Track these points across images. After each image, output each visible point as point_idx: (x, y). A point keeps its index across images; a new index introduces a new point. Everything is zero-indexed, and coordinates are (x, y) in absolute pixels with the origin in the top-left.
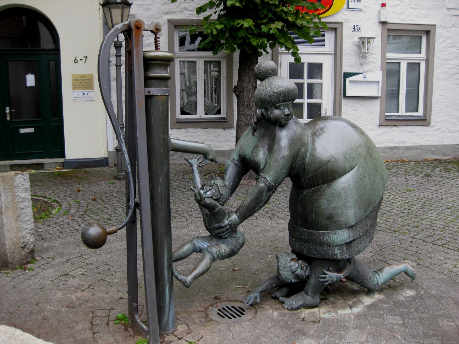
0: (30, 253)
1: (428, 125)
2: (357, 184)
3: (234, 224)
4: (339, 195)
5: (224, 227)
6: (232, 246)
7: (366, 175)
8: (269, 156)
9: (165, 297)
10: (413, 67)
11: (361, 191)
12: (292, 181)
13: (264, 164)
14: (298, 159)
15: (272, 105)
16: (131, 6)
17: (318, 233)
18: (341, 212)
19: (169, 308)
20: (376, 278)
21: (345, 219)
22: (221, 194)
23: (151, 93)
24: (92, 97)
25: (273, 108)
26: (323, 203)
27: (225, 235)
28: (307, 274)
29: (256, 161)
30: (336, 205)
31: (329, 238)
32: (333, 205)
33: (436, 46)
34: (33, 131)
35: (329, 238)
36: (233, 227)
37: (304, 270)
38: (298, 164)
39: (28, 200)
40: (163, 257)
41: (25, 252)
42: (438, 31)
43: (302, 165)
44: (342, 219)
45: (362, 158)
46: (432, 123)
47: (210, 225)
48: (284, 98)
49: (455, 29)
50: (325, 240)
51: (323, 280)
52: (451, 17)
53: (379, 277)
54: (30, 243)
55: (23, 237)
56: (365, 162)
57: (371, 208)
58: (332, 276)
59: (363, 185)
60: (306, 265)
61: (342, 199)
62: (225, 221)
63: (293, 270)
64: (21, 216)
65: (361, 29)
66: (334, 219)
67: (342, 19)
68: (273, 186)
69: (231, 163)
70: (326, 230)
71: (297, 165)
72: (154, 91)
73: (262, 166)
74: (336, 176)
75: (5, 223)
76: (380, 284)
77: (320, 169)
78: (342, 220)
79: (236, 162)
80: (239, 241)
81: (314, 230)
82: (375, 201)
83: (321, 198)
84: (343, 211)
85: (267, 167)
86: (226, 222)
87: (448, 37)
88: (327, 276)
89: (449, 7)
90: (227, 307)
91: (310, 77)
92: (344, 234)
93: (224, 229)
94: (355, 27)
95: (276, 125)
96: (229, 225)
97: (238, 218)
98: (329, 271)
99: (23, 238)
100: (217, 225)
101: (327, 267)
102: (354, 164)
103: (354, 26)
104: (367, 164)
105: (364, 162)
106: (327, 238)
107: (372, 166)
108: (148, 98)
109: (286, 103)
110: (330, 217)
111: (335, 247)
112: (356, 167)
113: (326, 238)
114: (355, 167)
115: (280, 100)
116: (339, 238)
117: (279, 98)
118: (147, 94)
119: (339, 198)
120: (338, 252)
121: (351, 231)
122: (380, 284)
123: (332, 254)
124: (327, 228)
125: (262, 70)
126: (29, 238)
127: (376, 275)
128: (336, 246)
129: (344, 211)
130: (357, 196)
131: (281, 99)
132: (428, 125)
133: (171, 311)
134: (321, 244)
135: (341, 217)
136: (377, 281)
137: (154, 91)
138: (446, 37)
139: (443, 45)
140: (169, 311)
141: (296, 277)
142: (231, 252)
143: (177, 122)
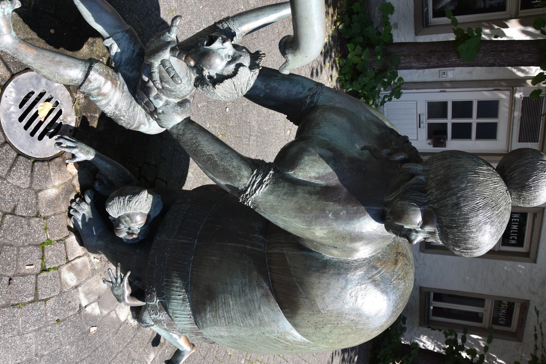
4: (250, 315)
18: (221, 315)
29: (301, 159)
30: (232, 307)
31: (177, 287)
32: (231, 303)
34: (453, 39)
46: (422, 254)
61: (244, 319)
66: (208, 302)
69: (307, 89)
78: (208, 316)
79: (308, 101)
84: (223, 318)
90: (60, 113)
92: (185, 316)
106: (178, 285)
116: (177, 307)
119: (245, 314)
120: (156, 302)
129: (223, 321)
135: (212, 315)
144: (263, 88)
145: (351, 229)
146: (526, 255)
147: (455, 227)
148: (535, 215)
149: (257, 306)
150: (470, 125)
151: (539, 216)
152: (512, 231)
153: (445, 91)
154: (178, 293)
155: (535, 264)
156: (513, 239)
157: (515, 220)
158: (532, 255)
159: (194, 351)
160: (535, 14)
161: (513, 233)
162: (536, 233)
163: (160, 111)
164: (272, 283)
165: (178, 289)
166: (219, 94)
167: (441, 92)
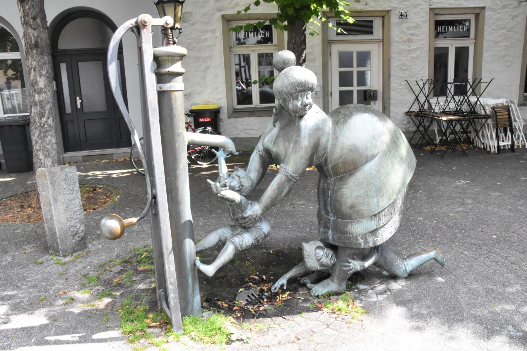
0: (80, 241)
5: (246, 218)
6: (256, 236)
15: (289, 95)
16: (184, 4)
20: (405, 265)
22: (242, 186)
23: (163, 89)
27: (249, 225)
28: (332, 262)
33: (485, 29)
37: (330, 258)
41: (75, 240)
42: (488, 13)
43: (324, 155)
44: (364, 208)
48: (301, 89)
49: (507, 10)
50: (348, 228)
51: (348, 268)
53: (408, 264)
54: (81, 232)
55: (72, 226)
58: (356, 265)
63: (318, 258)
64: (70, 207)
65: (409, 17)
66: (357, 208)
67: (389, 7)
73: (282, 157)
75: (54, 214)
77: (341, 158)
83: (344, 187)
87: (498, 19)
88: (351, 264)
91: (352, 66)
93: (247, 219)
94: (403, 14)
99: (73, 228)
102: (376, 152)
103: (402, 13)
108: (161, 94)
112: (379, 156)
114: (377, 155)
115: (296, 90)
118: (159, 90)
138: (496, 19)
139: (493, 27)
141: (322, 265)
143: (234, 112)
145: (308, 132)
146: (477, 16)
148: (436, 14)
150: (352, 72)
151: (437, 12)
152: (455, 31)
153: (331, 93)
155: (486, 8)
157: (443, 29)
158: (477, 11)
159: (39, 50)
161: (456, 29)
162: (455, 12)
164: (346, 173)
167: (331, 96)
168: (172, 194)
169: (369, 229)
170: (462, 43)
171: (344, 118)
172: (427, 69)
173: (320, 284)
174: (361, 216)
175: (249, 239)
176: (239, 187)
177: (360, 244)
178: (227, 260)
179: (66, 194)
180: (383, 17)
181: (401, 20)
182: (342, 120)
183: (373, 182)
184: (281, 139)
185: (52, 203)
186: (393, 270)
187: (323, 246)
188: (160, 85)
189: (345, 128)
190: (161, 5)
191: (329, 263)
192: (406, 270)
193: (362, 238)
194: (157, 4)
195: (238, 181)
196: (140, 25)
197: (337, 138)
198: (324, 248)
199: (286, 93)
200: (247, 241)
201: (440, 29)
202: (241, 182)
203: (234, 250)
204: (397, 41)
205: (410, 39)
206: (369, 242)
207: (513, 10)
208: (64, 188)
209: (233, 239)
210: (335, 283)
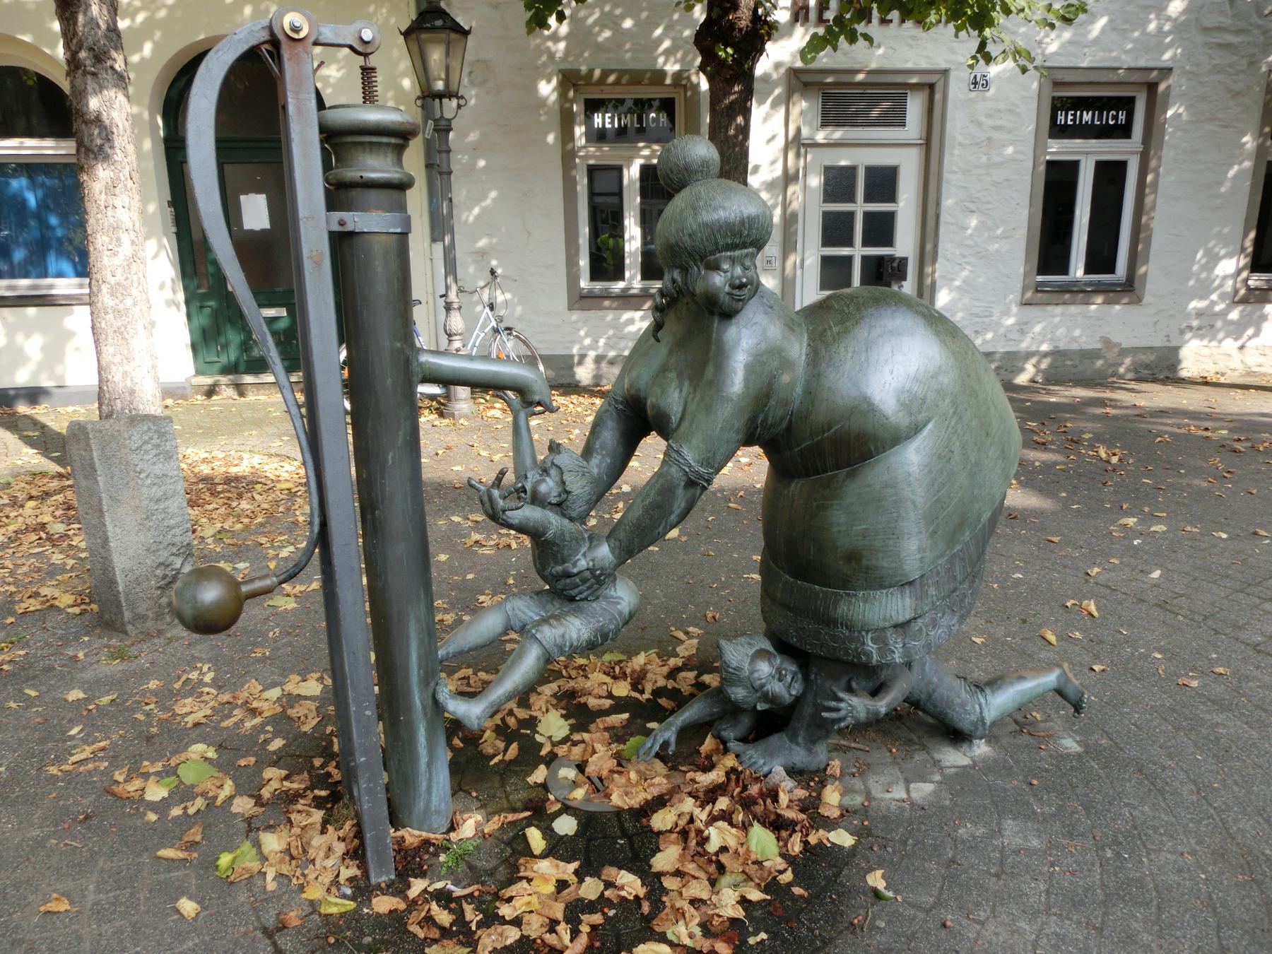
1: (1138, 300)
2: (930, 471)
3: (602, 569)
4: (879, 501)
7: (957, 447)
8: (691, 396)
9: (418, 753)
10: (1110, 174)
11: (938, 492)
12: (768, 454)
13: (679, 416)
14: (772, 402)
15: (697, 257)
17: (823, 592)
19: (430, 779)
21: (894, 565)
22: (568, 493)
24: (1101, 259)
25: (701, 267)
26: (838, 518)
27: (581, 593)
31: (849, 610)
32: (863, 527)
35: (849, 610)
36: (600, 575)
38: (771, 415)
39: (172, 481)
40: (408, 655)
45: (947, 401)
47: (544, 569)
48: (729, 241)
50: (839, 611)
51: (834, 715)
52: (1210, 48)
56: (954, 413)
57: (967, 533)
59: (945, 473)
60: (794, 668)
62: (579, 560)
66: (865, 562)
68: (701, 476)
70: (844, 587)
71: (770, 419)
72: (357, 221)
73: (674, 419)
74: (873, 448)
75: (110, 534)
76: (988, 721)
78: (885, 564)
79: (621, 407)
80: (619, 607)
81: (814, 583)
82: (979, 517)
83: (832, 505)
85: (686, 424)
86: (583, 564)
88: (842, 705)
89: (1207, 24)
94: (978, 79)
95: (712, 313)
96: (588, 569)
97: (613, 553)
98: (850, 690)
100: (559, 568)
101: (844, 681)
102: (921, 417)
103: (975, 77)
104: (960, 418)
105: (951, 411)
106: (845, 608)
107: (974, 423)
108: (341, 242)
109: (737, 253)
110: (853, 557)
111: (864, 633)
112: (930, 426)
113: (842, 609)
114: (925, 426)
115: (717, 243)
117: (716, 239)
118: (336, 228)
121: (908, 594)
122: (988, 721)
123: (856, 649)
124: (845, 584)
125: (676, 164)
126: (178, 566)
127: (980, 696)
128: (867, 632)
129: (891, 542)
130: (929, 504)
131: (721, 242)
132: (1138, 300)
133: (434, 785)
134: (831, 622)
136: (981, 713)
137: (357, 221)
140: (429, 787)
142: (596, 636)
144: (600, 457)
147: (715, 236)
149: (867, 489)
154: (856, 609)
156: (1115, 118)
160: (683, 109)
161: (1100, 119)
163: (591, 563)
165: (852, 608)
166: (580, 491)
168: (373, 514)
169: (894, 618)
170: (1110, 149)
171: (842, 322)
172: (1026, 213)
173: (762, 745)
174: (878, 581)
175: (579, 630)
176: (560, 495)
177: (869, 655)
178: (521, 688)
179: (143, 485)
180: (931, 87)
181: (973, 95)
182: (835, 329)
183: (911, 496)
184: (673, 375)
185: (105, 508)
186: (950, 716)
187: (772, 650)
188: (337, 215)
189: (842, 350)
190: (414, 36)
191: (787, 696)
192: (983, 719)
193: (874, 640)
194: (407, 34)
195: (557, 479)
196: (281, 37)
197: (819, 375)
198: (775, 657)
199: (689, 253)
200: (575, 636)
201: (1063, 118)
202: (564, 483)
203: (539, 658)
204: (960, 144)
205: (989, 139)
206: (894, 652)
207: (1235, 77)
208: (138, 469)
209: (537, 631)
210: (798, 744)
